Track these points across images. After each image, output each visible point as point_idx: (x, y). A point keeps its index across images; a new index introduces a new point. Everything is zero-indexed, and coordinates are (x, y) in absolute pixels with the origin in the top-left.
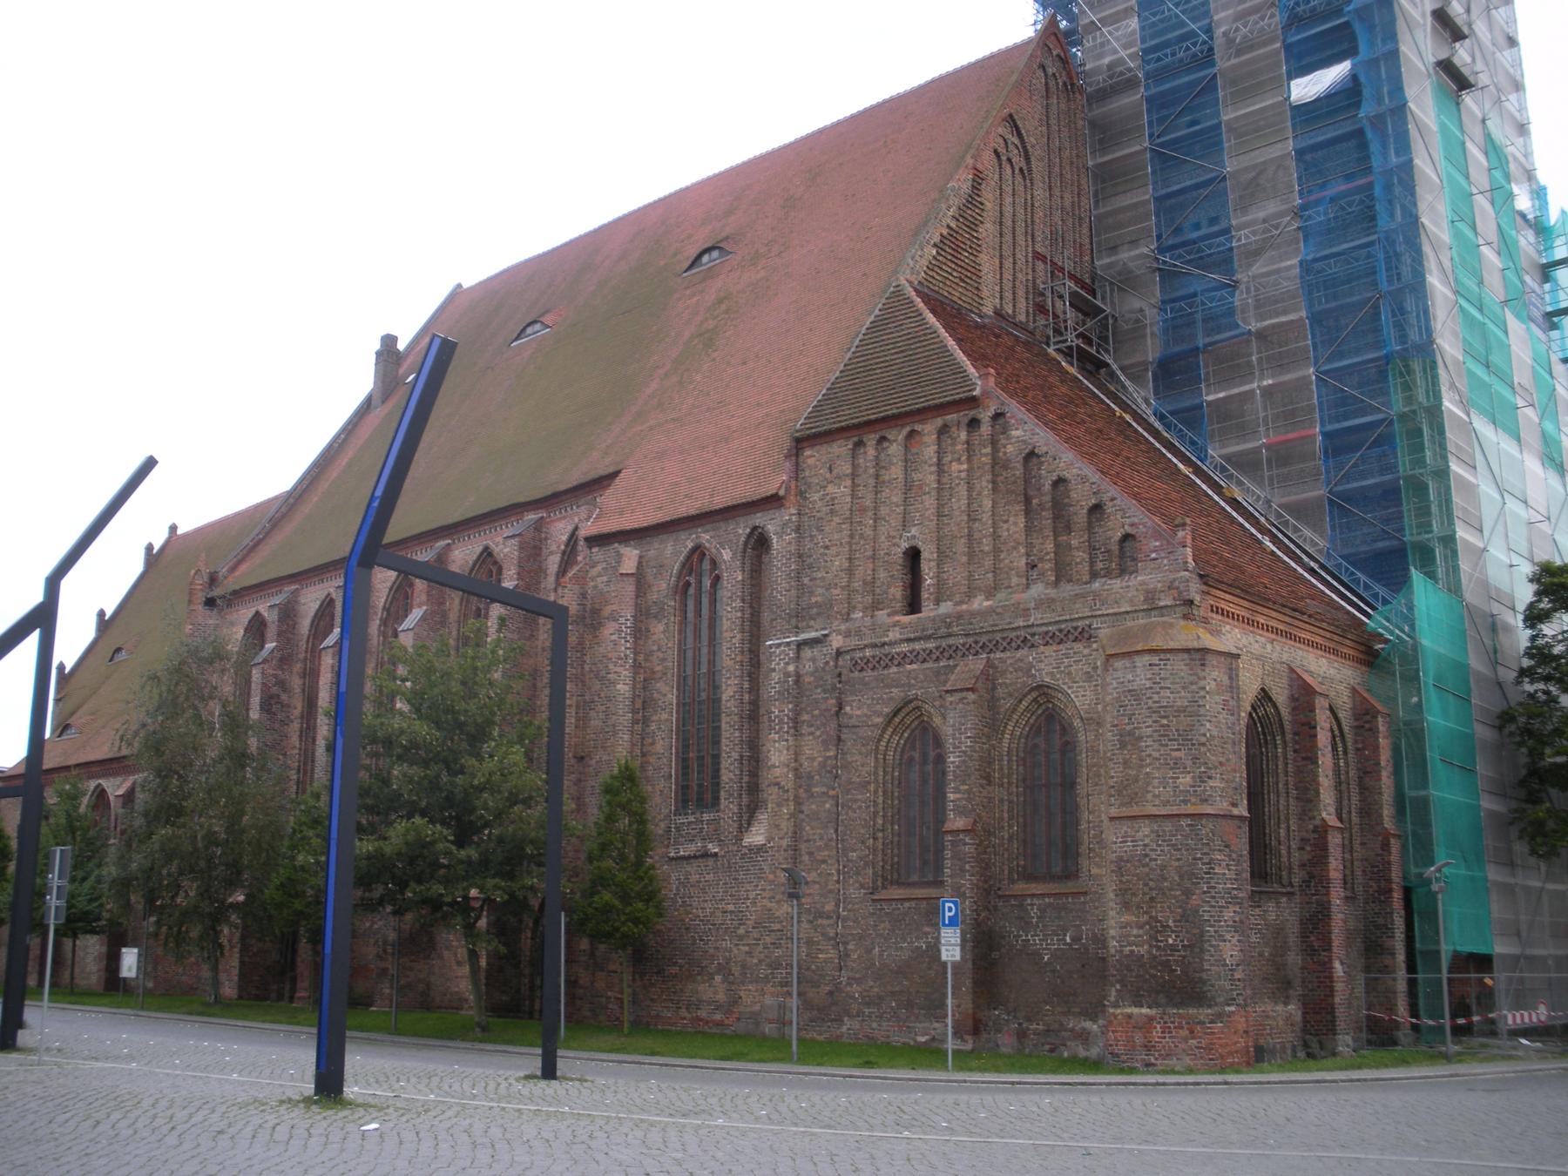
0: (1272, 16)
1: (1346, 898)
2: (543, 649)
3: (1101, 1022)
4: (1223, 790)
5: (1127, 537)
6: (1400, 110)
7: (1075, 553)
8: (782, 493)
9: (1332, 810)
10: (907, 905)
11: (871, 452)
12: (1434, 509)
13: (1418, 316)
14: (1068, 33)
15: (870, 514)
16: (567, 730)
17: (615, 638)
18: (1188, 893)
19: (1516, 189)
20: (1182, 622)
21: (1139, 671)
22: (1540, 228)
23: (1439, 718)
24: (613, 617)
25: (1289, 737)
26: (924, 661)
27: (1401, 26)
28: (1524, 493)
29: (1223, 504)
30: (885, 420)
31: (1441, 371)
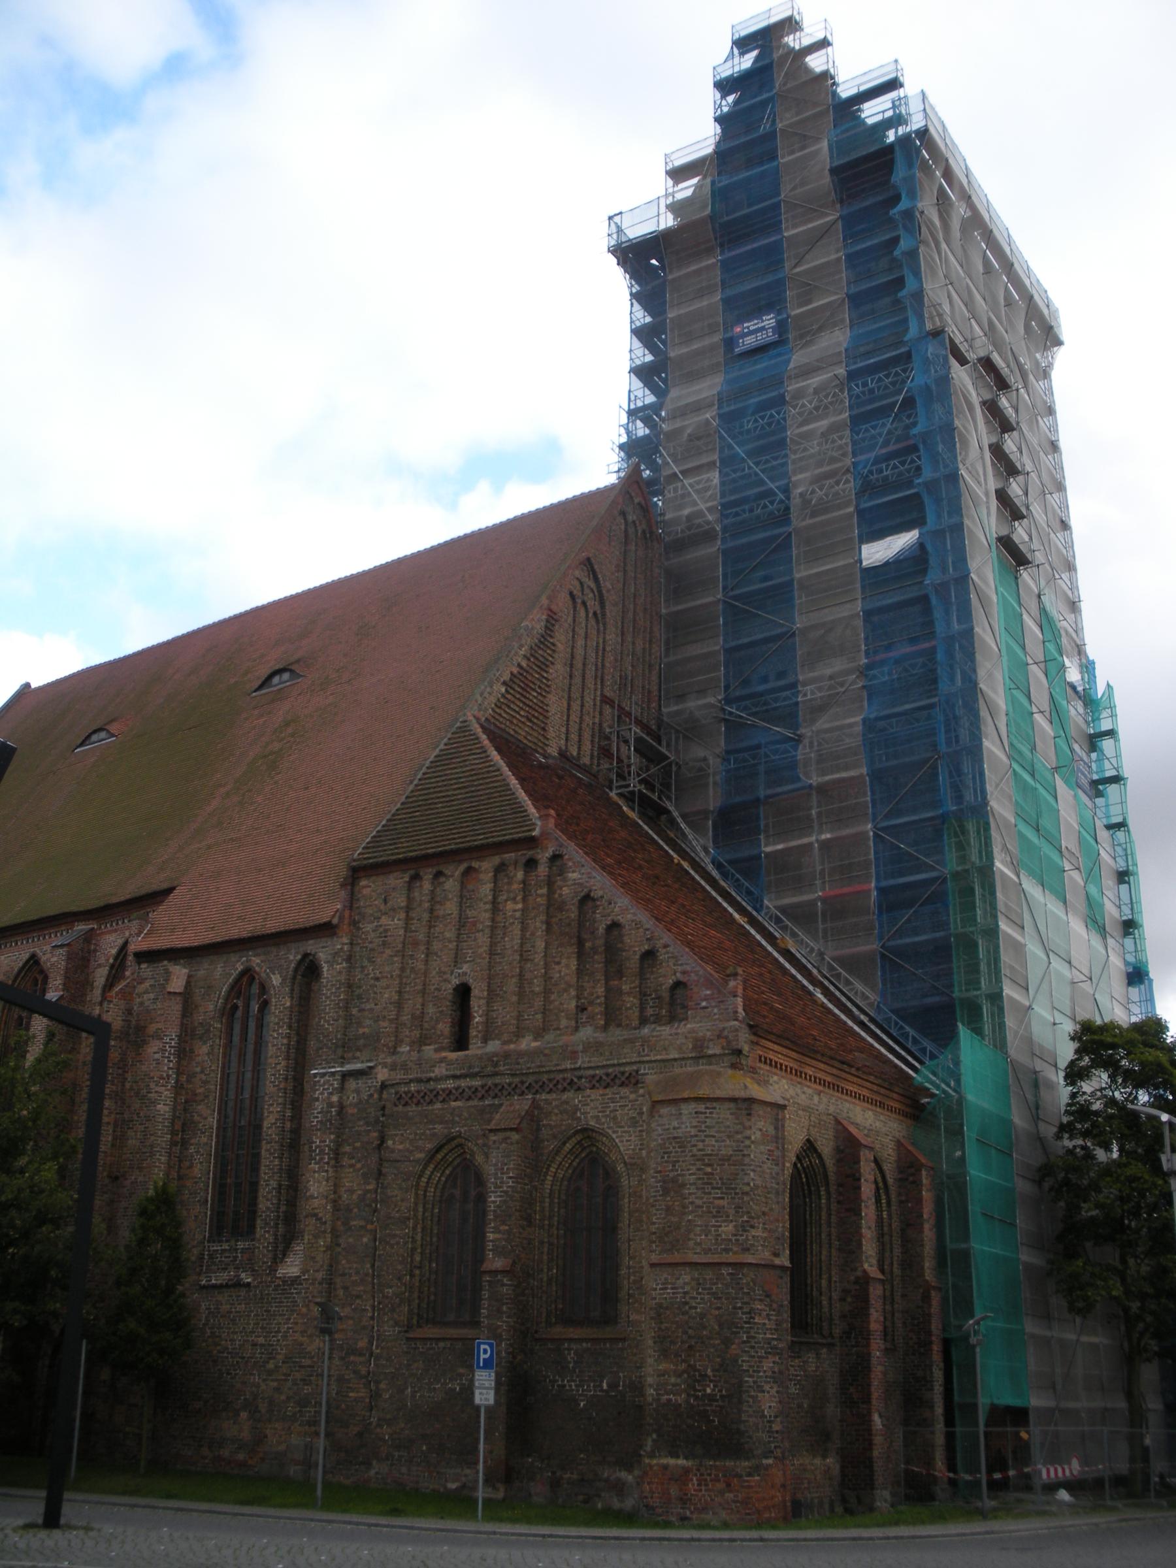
0: (847, 481)
1: (886, 1349)
2: (84, 1063)
3: (636, 1472)
4: (765, 1239)
5: (678, 984)
6: (963, 579)
7: (626, 998)
8: (335, 921)
9: (874, 1261)
10: (441, 1344)
11: (427, 886)
12: (983, 967)
13: (974, 778)
14: (650, 482)
15: (422, 948)
16: (103, 1148)
17: (159, 1056)
18: (727, 1342)
19: (1067, 663)
20: (730, 1072)
21: (684, 1118)
22: (1088, 700)
23: (978, 1172)
24: (158, 1036)
25: (833, 1188)
26: (470, 1098)
27: (966, 500)
28: (1069, 953)
29: (776, 954)
30: (441, 855)
31: (994, 833)
